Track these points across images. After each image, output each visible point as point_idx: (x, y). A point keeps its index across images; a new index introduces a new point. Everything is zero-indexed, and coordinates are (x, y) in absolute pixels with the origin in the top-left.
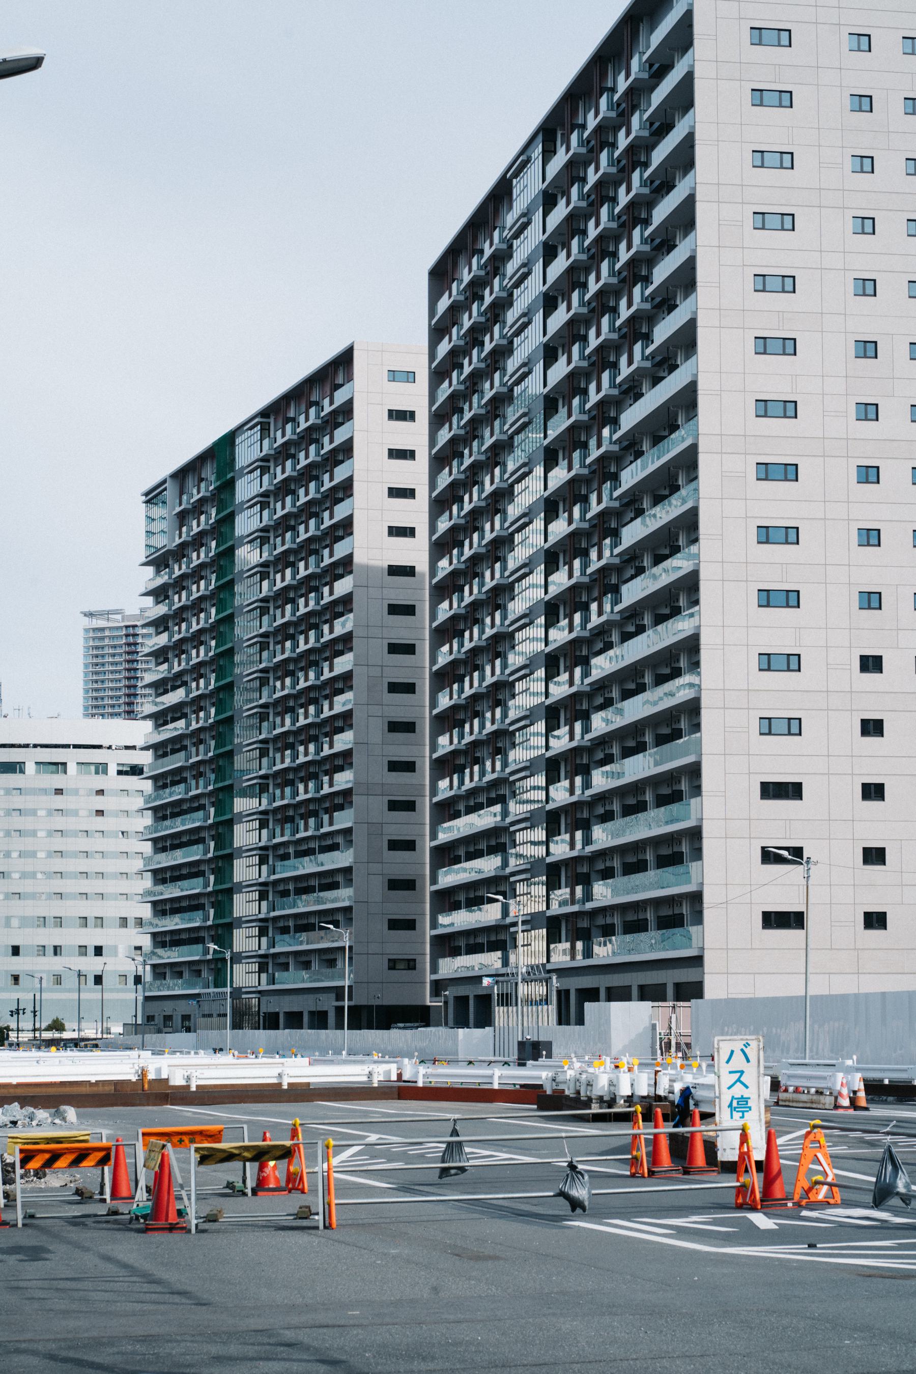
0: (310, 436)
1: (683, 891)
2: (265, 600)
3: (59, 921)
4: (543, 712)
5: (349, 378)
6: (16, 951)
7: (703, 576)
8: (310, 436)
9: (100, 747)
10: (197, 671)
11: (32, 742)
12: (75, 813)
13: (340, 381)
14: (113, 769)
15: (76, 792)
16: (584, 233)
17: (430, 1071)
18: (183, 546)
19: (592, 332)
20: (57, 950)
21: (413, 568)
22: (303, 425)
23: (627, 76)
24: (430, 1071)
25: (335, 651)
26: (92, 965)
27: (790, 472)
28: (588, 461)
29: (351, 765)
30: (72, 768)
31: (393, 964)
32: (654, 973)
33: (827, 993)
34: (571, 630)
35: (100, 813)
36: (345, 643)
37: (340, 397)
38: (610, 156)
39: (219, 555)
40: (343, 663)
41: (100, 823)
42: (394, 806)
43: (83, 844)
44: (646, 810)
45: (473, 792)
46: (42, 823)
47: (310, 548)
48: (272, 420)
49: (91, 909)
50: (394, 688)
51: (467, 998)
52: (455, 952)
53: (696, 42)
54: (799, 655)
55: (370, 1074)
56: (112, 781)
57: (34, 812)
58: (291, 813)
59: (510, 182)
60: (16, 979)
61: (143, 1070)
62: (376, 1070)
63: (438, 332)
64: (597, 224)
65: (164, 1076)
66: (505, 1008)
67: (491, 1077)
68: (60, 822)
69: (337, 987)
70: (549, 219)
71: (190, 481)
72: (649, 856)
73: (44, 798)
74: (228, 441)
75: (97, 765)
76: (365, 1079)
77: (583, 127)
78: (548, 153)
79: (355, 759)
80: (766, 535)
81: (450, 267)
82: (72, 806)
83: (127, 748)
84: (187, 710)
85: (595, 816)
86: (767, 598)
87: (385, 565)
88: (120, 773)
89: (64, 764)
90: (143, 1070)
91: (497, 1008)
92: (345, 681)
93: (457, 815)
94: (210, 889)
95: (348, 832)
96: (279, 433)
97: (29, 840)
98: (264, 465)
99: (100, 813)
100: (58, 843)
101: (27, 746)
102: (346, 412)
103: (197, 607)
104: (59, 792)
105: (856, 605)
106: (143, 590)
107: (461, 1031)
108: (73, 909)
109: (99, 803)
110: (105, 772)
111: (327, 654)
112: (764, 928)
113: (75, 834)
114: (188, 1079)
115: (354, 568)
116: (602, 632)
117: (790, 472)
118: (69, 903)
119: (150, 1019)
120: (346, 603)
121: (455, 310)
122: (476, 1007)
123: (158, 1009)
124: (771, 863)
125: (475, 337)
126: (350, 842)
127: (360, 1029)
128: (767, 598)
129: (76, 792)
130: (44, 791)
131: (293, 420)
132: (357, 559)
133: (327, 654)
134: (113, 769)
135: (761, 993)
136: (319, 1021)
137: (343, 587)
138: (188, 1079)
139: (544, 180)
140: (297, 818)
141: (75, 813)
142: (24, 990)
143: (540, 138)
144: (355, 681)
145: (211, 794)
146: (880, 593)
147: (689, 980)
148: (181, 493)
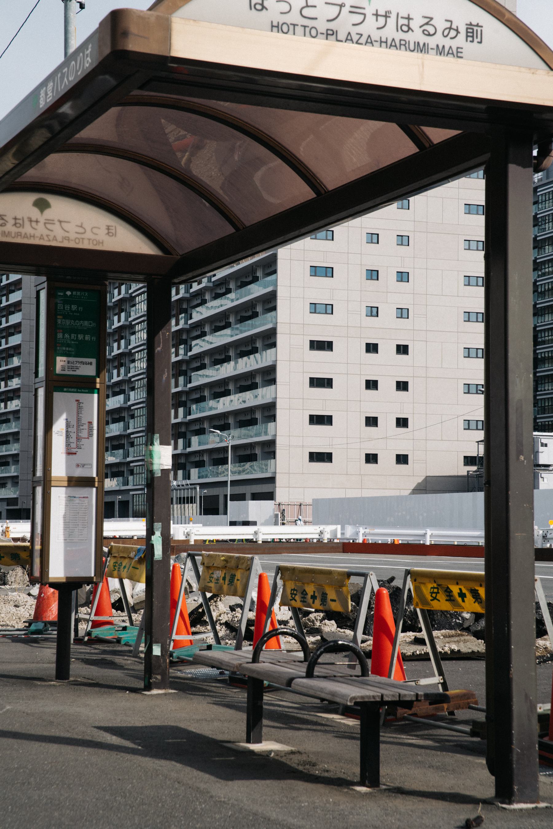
1: (258, 440)
17: (367, 531)
24: (367, 531)
25: (10, 311)
32: (241, 487)
44: (257, 388)
51: (113, 503)
54: (332, 305)
55: (321, 533)
62: (326, 530)
66: (182, 506)
67: (424, 535)
69: (7, 499)
72: (231, 421)
79: (22, 372)
85: (190, 400)
91: (175, 506)
112: (310, 461)
124: (314, 424)
126: (18, 418)
138: (188, 535)
144: (23, 328)
146: (378, 271)
147: (263, 491)
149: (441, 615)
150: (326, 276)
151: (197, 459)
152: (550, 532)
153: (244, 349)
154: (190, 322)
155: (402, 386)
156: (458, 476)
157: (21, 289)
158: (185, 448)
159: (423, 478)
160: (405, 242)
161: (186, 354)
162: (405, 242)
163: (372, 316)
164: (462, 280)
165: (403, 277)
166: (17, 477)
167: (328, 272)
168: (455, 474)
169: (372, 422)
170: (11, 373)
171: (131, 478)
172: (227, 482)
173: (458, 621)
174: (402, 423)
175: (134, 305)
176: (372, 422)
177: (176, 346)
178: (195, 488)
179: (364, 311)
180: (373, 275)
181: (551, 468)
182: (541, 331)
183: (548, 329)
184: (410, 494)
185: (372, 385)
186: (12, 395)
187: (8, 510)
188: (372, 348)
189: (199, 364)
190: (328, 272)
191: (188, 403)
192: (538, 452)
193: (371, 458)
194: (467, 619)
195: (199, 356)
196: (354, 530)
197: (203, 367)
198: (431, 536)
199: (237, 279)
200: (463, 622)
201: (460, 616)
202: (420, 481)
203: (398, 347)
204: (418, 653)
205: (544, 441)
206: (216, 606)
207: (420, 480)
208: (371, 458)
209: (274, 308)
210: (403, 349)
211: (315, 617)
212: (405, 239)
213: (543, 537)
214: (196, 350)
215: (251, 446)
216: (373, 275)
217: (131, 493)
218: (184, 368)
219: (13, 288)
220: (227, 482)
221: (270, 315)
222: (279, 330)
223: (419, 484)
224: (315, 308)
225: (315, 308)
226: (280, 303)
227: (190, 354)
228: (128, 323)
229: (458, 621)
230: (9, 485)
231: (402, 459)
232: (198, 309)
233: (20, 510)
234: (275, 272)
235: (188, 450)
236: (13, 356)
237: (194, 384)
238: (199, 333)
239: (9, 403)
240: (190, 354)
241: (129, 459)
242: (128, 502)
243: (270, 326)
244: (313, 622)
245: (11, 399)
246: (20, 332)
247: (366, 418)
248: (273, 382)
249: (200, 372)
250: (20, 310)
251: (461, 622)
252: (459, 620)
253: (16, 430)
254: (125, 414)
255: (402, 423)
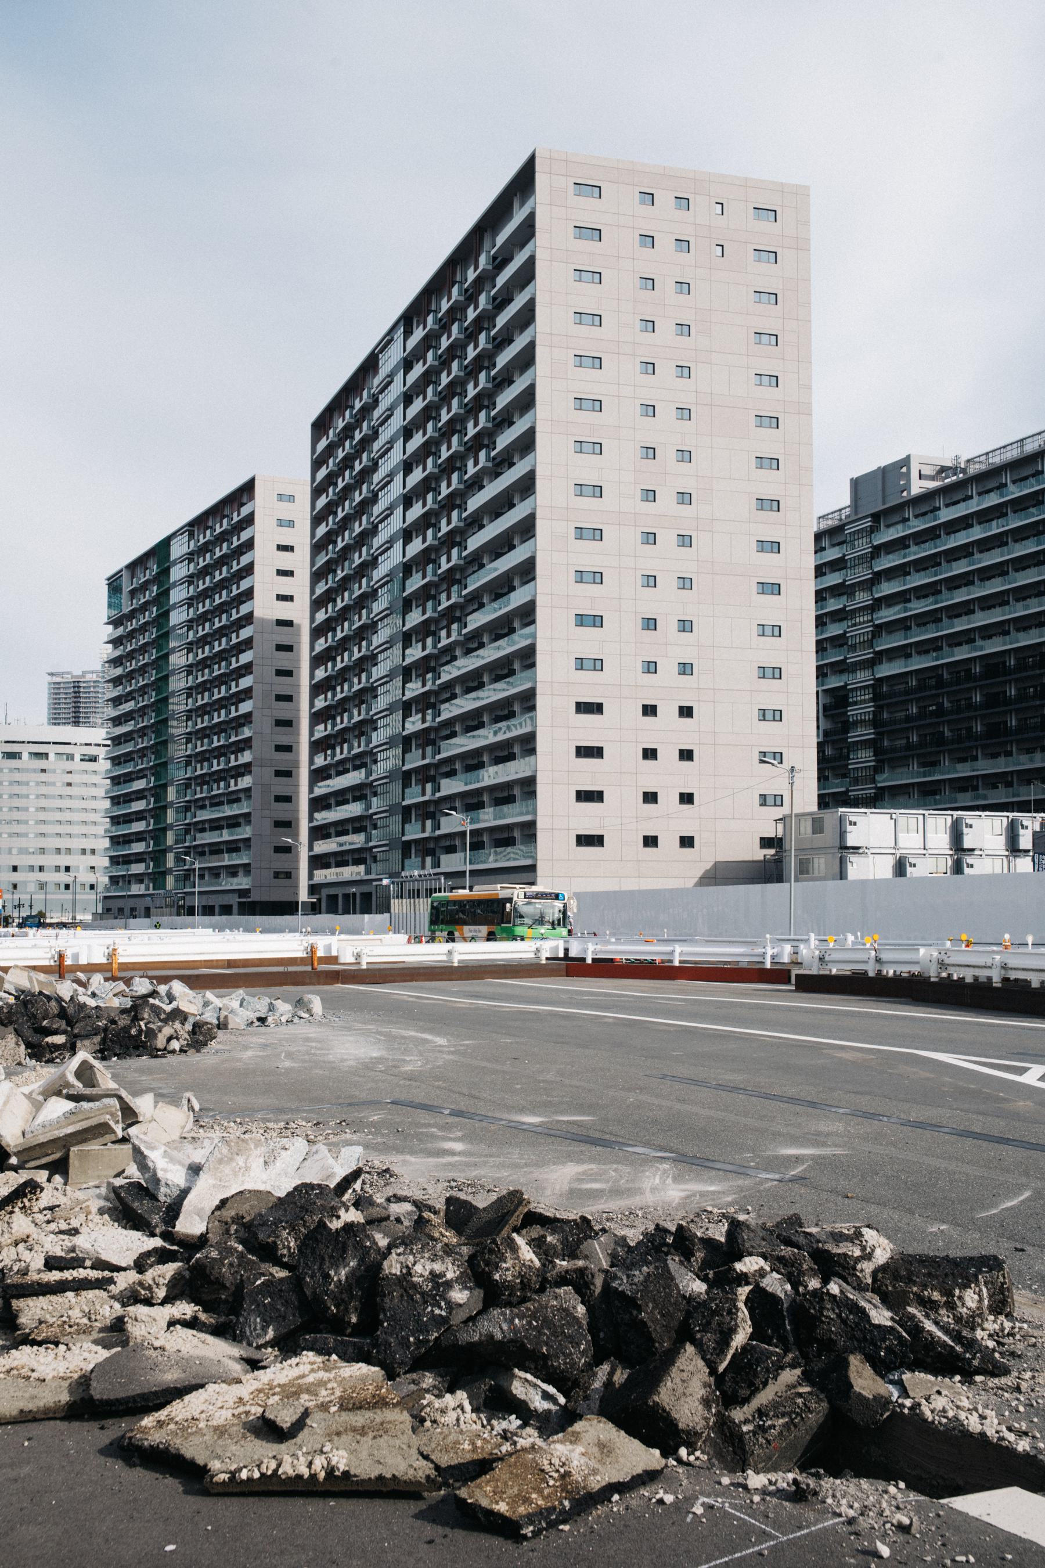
0: (224, 537)
2: (191, 643)
3: (42, 851)
4: (401, 704)
5: (251, 497)
6: (15, 869)
7: (538, 603)
8: (224, 537)
9: (69, 744)
10: (143, 690)
11: (26, 740)
12: (54, 784)
13: (244, 501)
14: (77, 758)
15: (54, 771)
16: (336, 484)
18: (133, 611)
19: (340, 539)
20: (41, 869)
21: (292, 622)
22: (218, 530)
23: (361, 400)
24: (599, 947)
26: (63, 878)
27: (597, 534)
28: (353, 597)
29: (250, 747)
30: (52, 756)
31: (277, 875)
33: (871, 877)
34: (326, 701)
35: (69, 784)
36: (247, 669)
37: (245, 511)
38: (435, 354)
39: (158, 616)
40: (245, 682)
41: (69, 791)
42: (278, 773)
43: (59, 803)
45: (342, 762)
46: (33, 790)
47: (223, 609)
48: (196, 529)
49: (63, 843)
50: (279, 698)
51: (336, 896)
52: (327, 866)
53: (537, 234)
55: (538, 950)
56: (77, 764)
57: (27, 784)
58: (207, 779)
59: (377, 356)
60: (15, 886)
61: (312, 947)
63: (317, 463)
64: (361, 463)
65: (334, 953)
67: (672, 953)
68: (43, 790)
70: (408, 377)
71: (138, 570)
73: (33, 775)
74: (165, 545)
75: (68, 755)
76: (532, 955)
77: (353, 407)
78: (408, 333)
80: (581, 576)
81: (328, 419)
82: (51, 780)
83: (86, 744)
84: (136, 715)
86: (581, 620)
87: (275, 618)
88: (82, 760)
89: (47, 754)
90: (312, 947)
92: (247, 694)
93: (329, 777)
94: (151, 828)
95: (247, 790)
96: (201, 536)
97: (24, 800)
98: (190, 557)
99: (69, 784)
100: (43, 803)
101: (23, 742)
102: (249, 520)
103: (143, 649)
104: (43, 771)
105: (640, 626)
106: (106, 640)
107: (366, 916)
108: (52, 843)
109: (69, 778)
110: (73, 759)
111: (234, 676)
113: (53, 797)
114: (358, 956)
115: (255, 620)
116: (449, 649)
117: (597, 534)
118: (49, 839)
119: (109, 910)
120: (248, 644)
121: (330, 449)
122: (361, 899)
123: (115, 905)
125: (347, 463)
127: (254, 914)
128: (581, 620)
129: (54, 771)
130: (35, 771)
131: (211, 527)
132: (256, 614)
133: (234, 676)
134: (77, 758)
135: (643, 887)
136: (226, 910)
137: (245, 633)
138: (358, 956)
139: (404, 351)
140: (211, 783)
141: (54, 784)
142: (21, 893)
143: (402, 322)
144: (254, 693)
145: (151, 768)
148: (133, 578)
149: (402, 1296)
150: (594, 626)
151: (448, 843)
152: (829, 952)
153: (502, 713)
154: (438, 682)
155: (686, 755)
156: (753, 862)
157: (252, 648)
158: (433, 831)
159: (711, 864)
160: (688, 585)
161: (433, 720)
162: (688, 585)
163: (649, 672)
164: (755, 630)
165: (685, 626)
166: (249, 865)
167: (597, 621)
168: (750, 859)
169: (650, 798)
170: (242, 745)
171: (373, 865)
172: (465, 872)
173: (437, 1311)
174: (687, 798)
175: (376, 664)
176: (650, 798)
177: (359, 707)
178: (439, 879)
179: (639, 667)
180: (650, 624)
181: (861, 851)
182: (852, 689)
183: (861, 687)
184: (696, 885)
185: (650, 754)
186: (243, 770)
187: (239, 903)
188: (650, 710)
189: (448, 732)
190: (597, 621)
191: (438, 777)
192: (845, 832)
193: (650, 841)
194: (460, 1305)
195: (449, 723)
196: (580, 947)
197: (453, 735)
198: (681, 954)
199: (491, 632)
200: (450, 1313)
201: (445, 1299)
202: (708, 868)
203: (681, 708)
204: (244, 1475)
205: (853, 819)
206: (8, 1223)
207: (708, 866)
208: (650, 841)
209: (533, 665)
210: (686, 712)
211: (154, 1279)
212: (688, 582)
213: (820, 959)
214: (445, 716)
215: (509, 827)
216: (650, 624)
217: (374, 883)
218: (432, 736)
219: (243, 648)
220: (465, 872)
221: (527, 673)
222: (538, 691)
223: (707, 871)
224: (581, 664)
225: (581, 664)
226: (540, 658)
227: (438, 720)
228: (369, 685)
229: (437, 1311)
230: (241, 874)
231: (687, 842)
232: (446, 668)
233: (254, 903)
234: (533, 622)
235: (438, 833)
236: (243, 725)
237: (443, 755)
238: (448, 695)
239: (239, 779)
240: (438, 720)
241: (371, 844)
242: (370, 894)
243: (528, 685)
244: (150, 1288)
245: (243, 775)
246: (251, 698)
247: (644, 793)
248: (533, 752)
249: (453, 741)
250: (251, 673)
251: (444, 1313)
252: (441, 1308)
253: (247, 811)
254: (367, 791)
255: (687, 798)
